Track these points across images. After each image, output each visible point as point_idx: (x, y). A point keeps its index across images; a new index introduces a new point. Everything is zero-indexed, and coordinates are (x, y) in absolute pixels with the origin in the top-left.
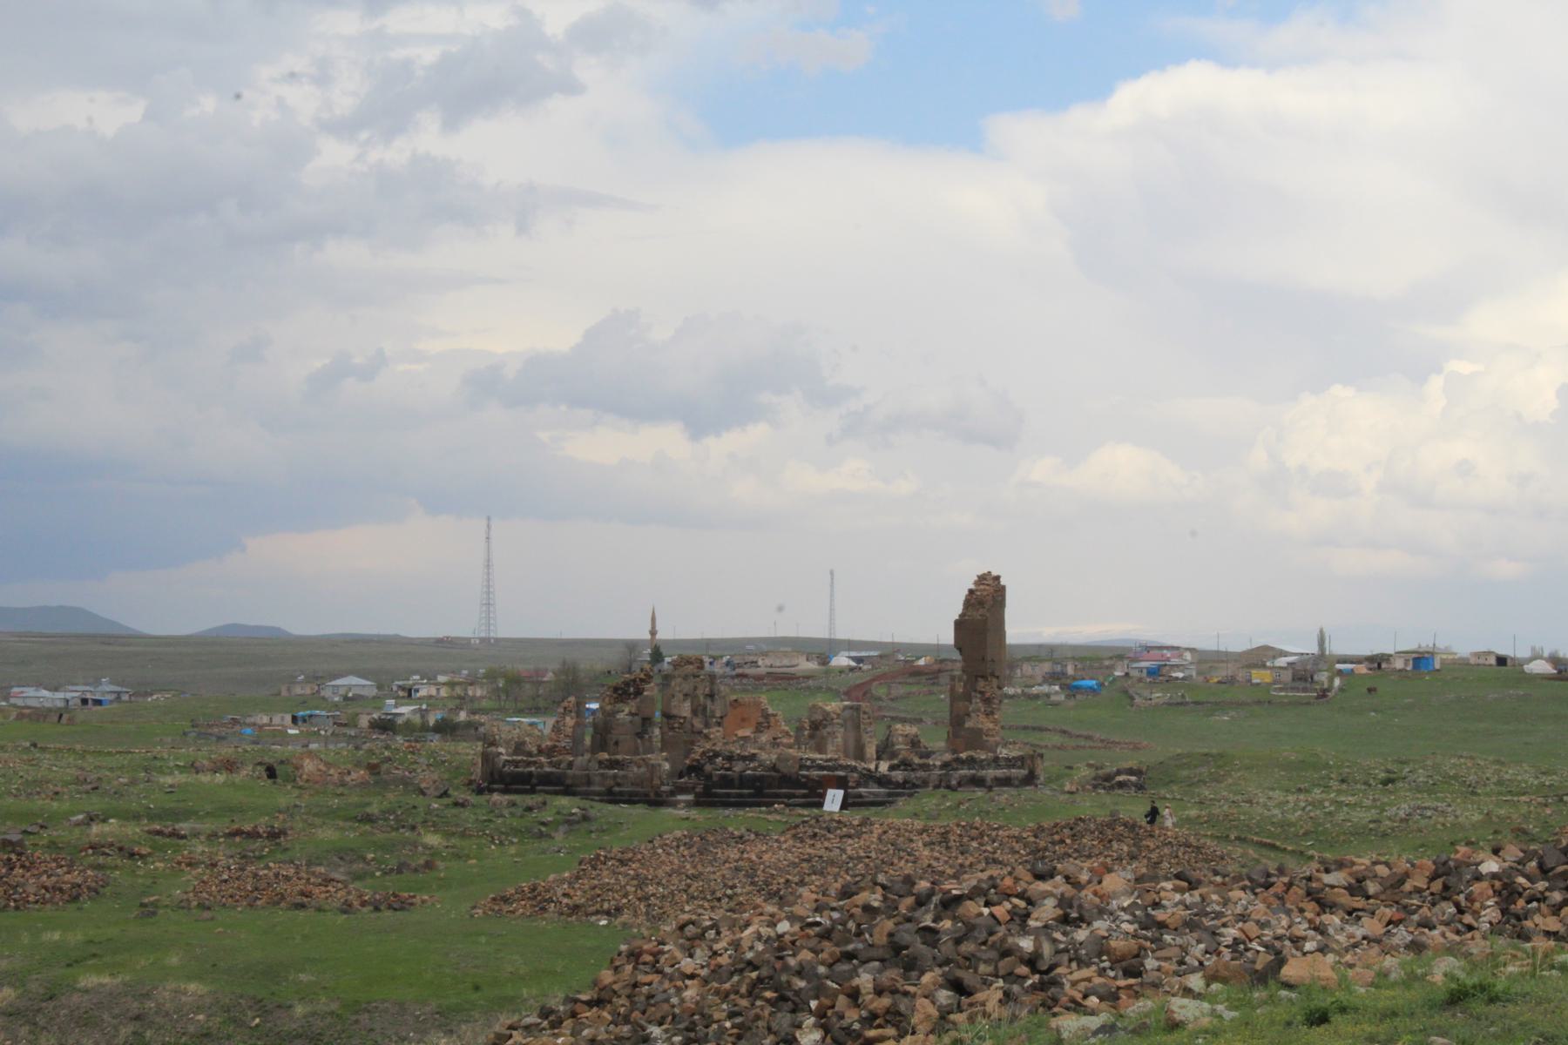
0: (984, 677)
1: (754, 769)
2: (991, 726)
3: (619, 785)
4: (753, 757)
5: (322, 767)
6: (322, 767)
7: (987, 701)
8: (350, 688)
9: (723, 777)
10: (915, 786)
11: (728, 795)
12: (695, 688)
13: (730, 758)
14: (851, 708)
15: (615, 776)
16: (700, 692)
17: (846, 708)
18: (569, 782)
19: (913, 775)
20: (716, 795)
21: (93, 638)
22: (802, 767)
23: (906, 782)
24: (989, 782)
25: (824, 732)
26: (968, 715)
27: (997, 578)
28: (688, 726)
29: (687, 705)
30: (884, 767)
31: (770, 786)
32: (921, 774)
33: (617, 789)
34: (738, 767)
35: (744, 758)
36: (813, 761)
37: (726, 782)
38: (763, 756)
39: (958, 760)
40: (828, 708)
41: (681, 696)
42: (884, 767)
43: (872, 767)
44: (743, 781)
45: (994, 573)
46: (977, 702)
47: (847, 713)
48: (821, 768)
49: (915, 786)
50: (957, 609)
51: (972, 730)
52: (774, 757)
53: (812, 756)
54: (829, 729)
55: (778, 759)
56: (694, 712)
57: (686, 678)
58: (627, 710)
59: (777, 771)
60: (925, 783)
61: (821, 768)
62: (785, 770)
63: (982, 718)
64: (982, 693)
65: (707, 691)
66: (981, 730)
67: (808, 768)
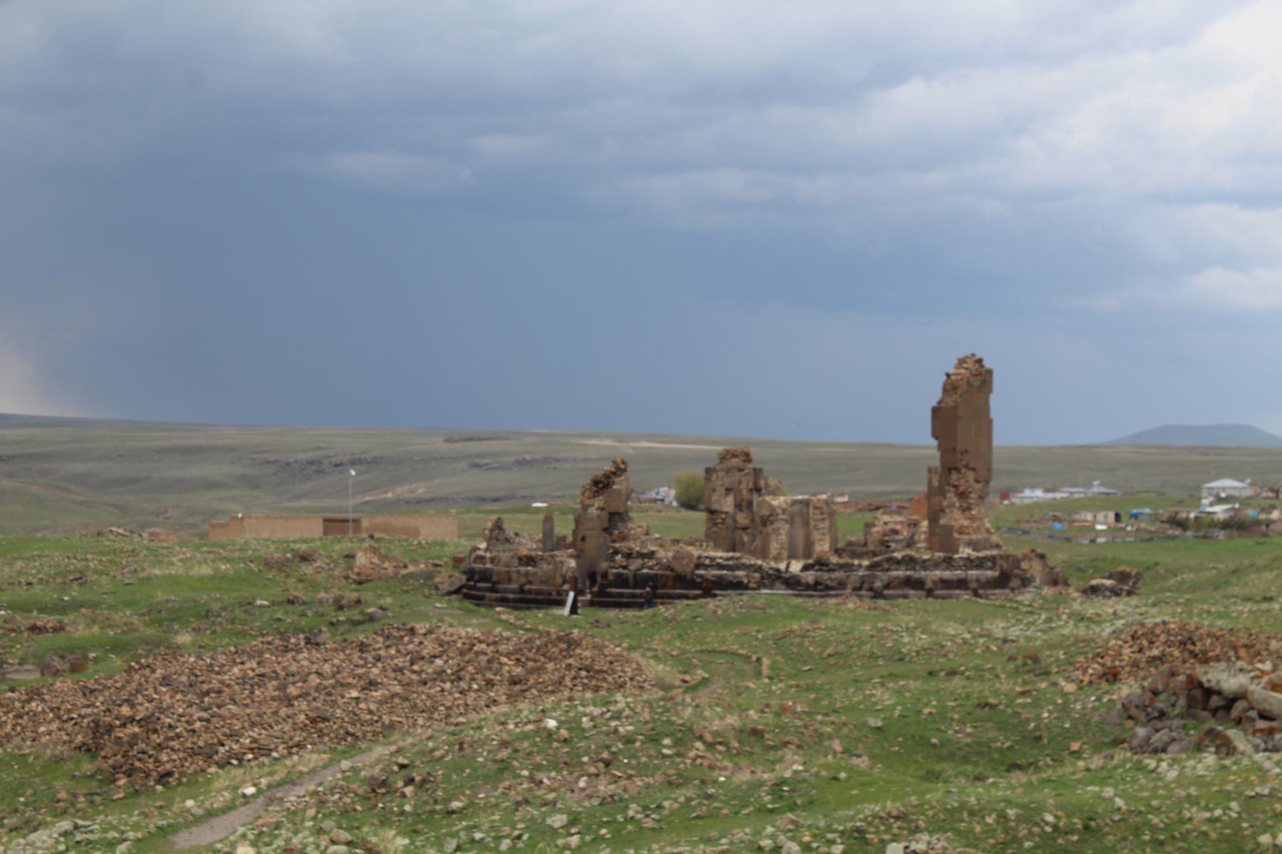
0: (957, 469)
1: (651, 568)
2: (966, 523)
3: (530, 582)
4: (651, 555)
5: (376, 560)
6: (376, 560)
7: (962, 495)
8: (1224, 489)
9: (619, 576)
10: (828, 588)
11: (621, 595)
12: (740, 483)
13: (629, 556)
14: (801, 502)
15: (527, 574)
16: (743, 486)
17: (794, 502)
18: (495, 579)
19: (826, 576)
20: (610, 595)
21: (1193, 450)
22: (698, 566)
23: (817, 583)
24: (929, 584)
25: (770, 529)
26: (943, 511)
27: (979, 361)
28: (729, 522)
29: (730, 499)
30: (796, 567)
31: (664, 587)
32: (839, 575)
33: (527, 587)
34: (635, 564)
35: (642, 556)
36: (712, 559)
37: (621, 581)
38: (661, 554)
39: (890, 560)
40: (775, 503)
41: (723, 491)
42: (796, 567)
43: (782, 566)
44: (639, 581)
45: (978, 356)
46: (951, 497)
47: (797, 508)
48: (720, 567)
49: (828, 588)
50: (935, 395)
51: (945, 526)
52: (670, 554)
53: (712, 554)
54: (774, 526)
55: (674, 557)
56: (739, 507)
57: (728, 471)
58: (596, 504)
59: (672, 570)
60: (842, 585)
61: (720, 567)
62: (679, 569)
63: (957, 514)
64: (955, 486)
65: (751, 485)
66: (952, 527)
67: (706, 567)
